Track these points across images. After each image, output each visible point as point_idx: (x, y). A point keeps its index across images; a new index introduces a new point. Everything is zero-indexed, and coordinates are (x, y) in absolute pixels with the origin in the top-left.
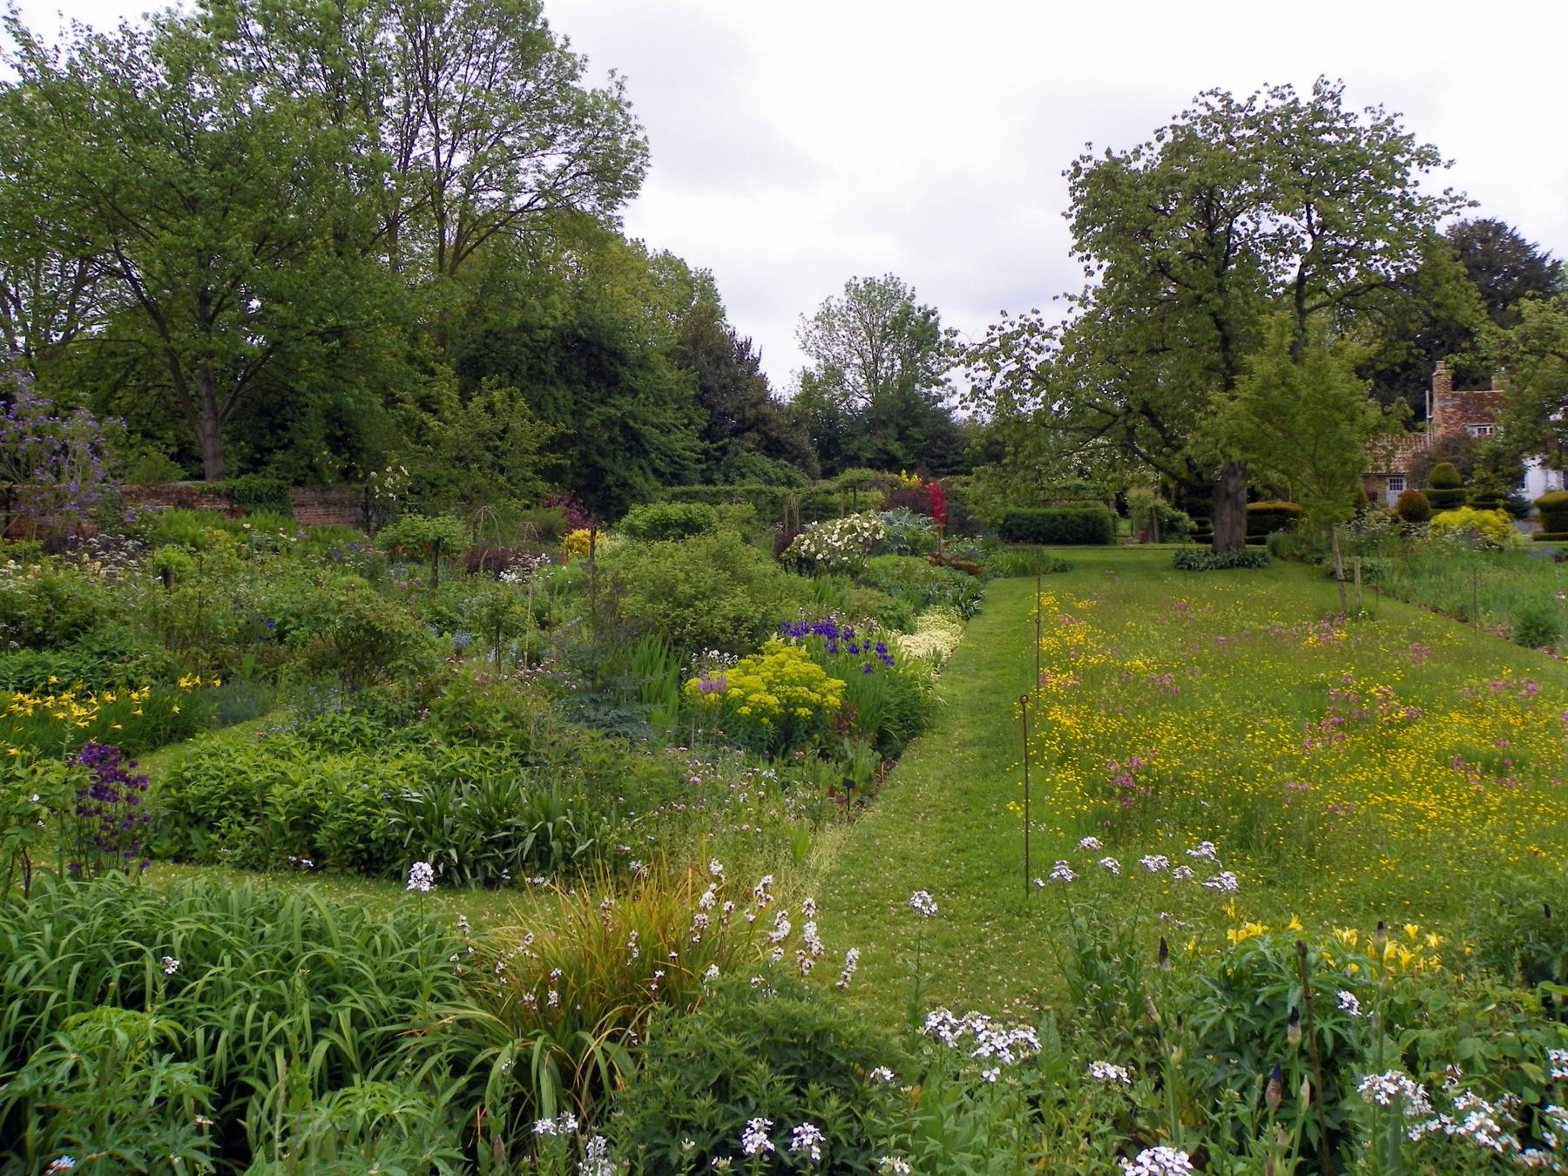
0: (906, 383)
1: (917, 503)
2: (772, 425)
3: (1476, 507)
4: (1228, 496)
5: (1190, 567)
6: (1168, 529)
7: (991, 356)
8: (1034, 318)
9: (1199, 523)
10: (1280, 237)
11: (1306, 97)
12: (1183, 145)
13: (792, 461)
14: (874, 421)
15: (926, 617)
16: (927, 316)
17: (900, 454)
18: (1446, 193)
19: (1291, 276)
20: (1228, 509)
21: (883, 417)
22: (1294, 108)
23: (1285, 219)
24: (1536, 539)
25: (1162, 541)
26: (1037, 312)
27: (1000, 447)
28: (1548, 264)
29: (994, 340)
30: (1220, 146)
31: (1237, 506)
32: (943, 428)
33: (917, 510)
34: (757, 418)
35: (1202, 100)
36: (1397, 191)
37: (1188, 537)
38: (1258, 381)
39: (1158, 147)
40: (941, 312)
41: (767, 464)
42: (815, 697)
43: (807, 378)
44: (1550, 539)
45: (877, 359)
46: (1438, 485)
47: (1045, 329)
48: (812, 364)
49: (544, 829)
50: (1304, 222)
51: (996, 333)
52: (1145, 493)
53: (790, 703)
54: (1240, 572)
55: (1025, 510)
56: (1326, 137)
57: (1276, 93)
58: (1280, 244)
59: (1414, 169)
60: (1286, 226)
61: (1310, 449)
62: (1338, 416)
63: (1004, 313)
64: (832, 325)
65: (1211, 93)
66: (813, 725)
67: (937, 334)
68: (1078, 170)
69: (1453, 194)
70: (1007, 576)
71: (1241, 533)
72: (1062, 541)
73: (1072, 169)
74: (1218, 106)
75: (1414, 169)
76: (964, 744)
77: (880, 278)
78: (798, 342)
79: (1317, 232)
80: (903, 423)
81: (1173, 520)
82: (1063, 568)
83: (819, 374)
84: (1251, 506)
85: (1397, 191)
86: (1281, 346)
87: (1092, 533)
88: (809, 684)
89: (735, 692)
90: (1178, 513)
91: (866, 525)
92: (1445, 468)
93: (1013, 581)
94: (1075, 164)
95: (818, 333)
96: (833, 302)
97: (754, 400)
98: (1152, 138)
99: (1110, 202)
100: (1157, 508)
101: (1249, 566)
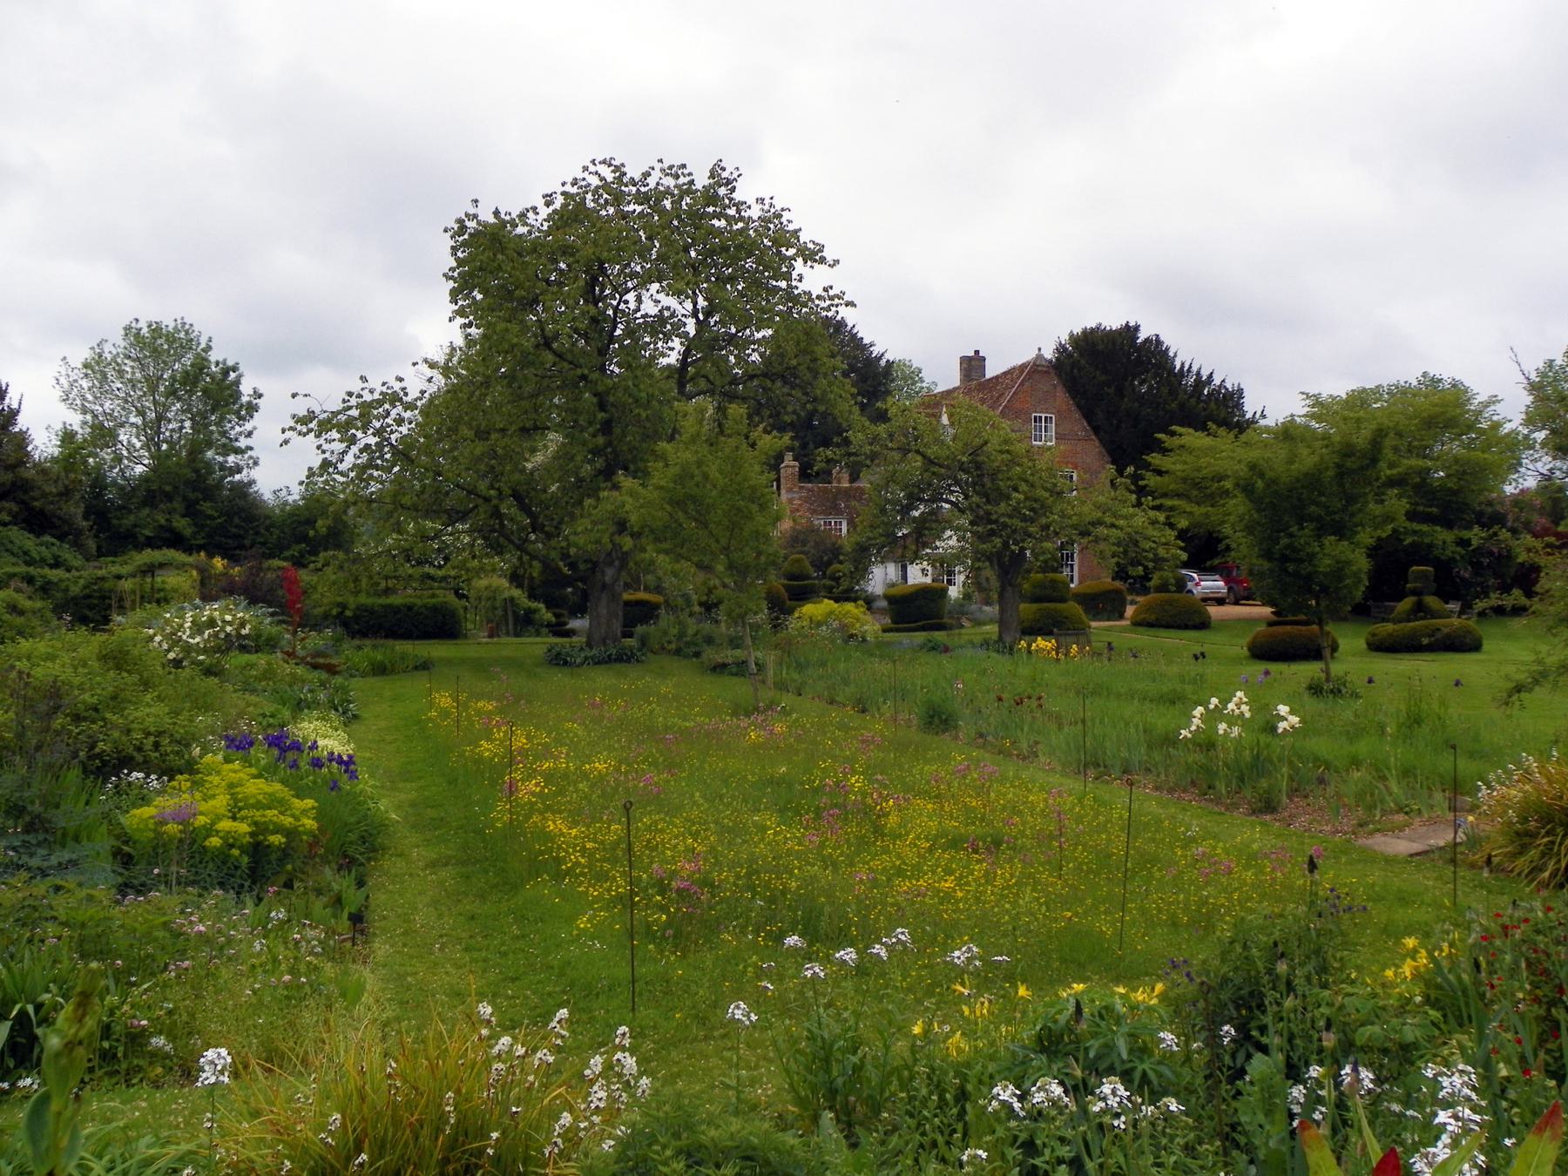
0: (196, 450)
1: (253, 594)
2: (36, 493)
3: (837, 600)
4: (604, 586)
5: (566, 663)
6: (524, 623)
7: (344, 427)
8: (397, 386)
9: (556, 615)
10: (661, 319)
11: (702, 180)
12: (571, 212)
13: (61, 537)
14: (150, 492)
15: (305, 724)
16: (226, 372)
17: (188, 532)
18: (825, 290)
19: (672, 359)
20: (604, 602)
21: (168, 488)
22: (688, 189)
23: (671, 302)
24: (884, 631)
25: (517, 635)
26: (400, 380)
27: (311, 529)
28: (883, 362)
29: (350, 408)
30: (609, 219)
31: (615, 597)
32: (241, 503)
33: (253, 601)
34: (13, 484)
35: (592, 168)
36: (783, 284)
37: (545, 630)
38: (674, 471)
39: (544, 212)
40: (242, 368)
41: (27, 541)
42: (287, 821)
43: (68, 437)
44: (898, 630)
45: (160, 418)
46: (792, 577)
47: (408, 399)
48: (75, 420)
49: (23, 1014)
50: (689, 305)
51: (353, 401)
52: (494, 580)
53: (260, 829)
54: (617, 666)
55: (370, 601)
56: (716, 222)
57: (671, 171)
58: (661, 325)
59: (799, 264)
60: (668, 308)
61: (723, 542)
62: (754, 508)
63: (364, 379)
64: (104, 375)
65: (604, 162)
66: (285, 853)
67: (238, 394)
68: (462, 228)
69: (831, 293)
70: (364, 675)
71: (617, 627)
72: (407, 636)
73: (456, 226)
74: (610, 177)
75: (799, 264)
76: (433, 865)
77: (168, 323)
78: (58, 393)
79: (701, 317)
80: (192, 496)
81: (530, 612)
82: (424, 666)
83: (82, 432)
84: (626, 596)
85: (783, 284)
86: (698, 435)
87: (442, 626)
88: (274, 802)
89: (201, 820)
90: (534, 605)
91: (228, 618)
92: (798, 561)
93: (371, 680)
94: (460, 221)
95: (85, 384)
96: (107, 348)
97: (12, 461)
98: (540, 203)
99: (492, 263)
100: (512, 599)
101: (628, 661)
